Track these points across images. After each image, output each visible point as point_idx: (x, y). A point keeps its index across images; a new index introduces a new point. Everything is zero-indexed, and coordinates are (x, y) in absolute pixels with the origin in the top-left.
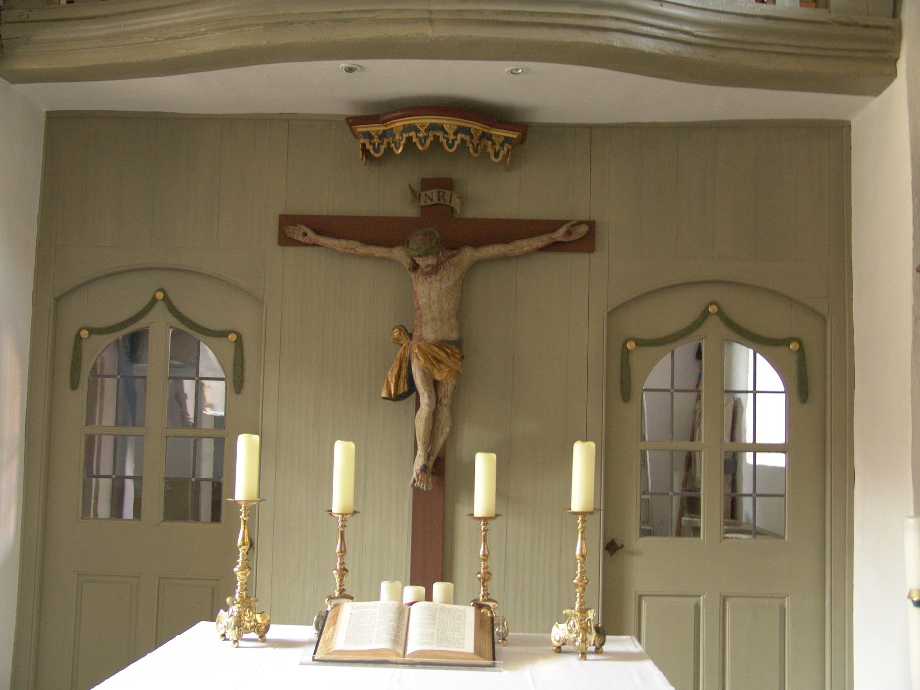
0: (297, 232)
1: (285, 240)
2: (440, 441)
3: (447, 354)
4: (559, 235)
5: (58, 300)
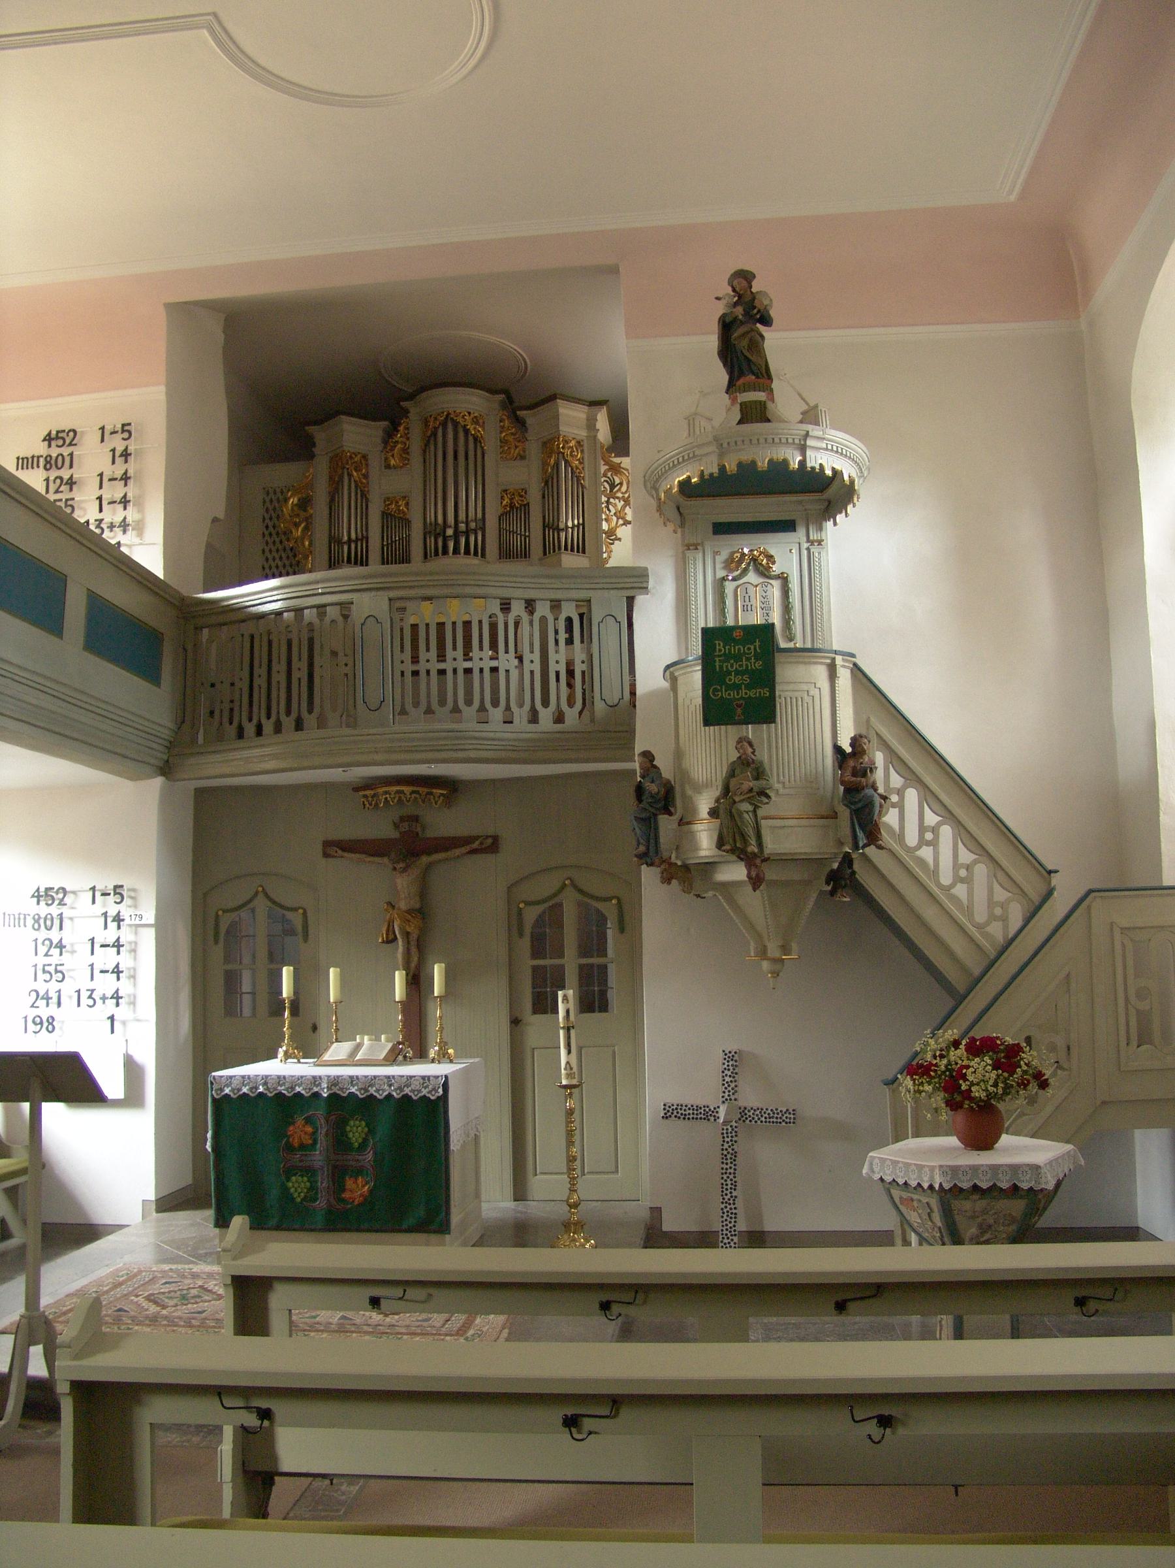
0: (332, 850)
2: (413, 965)
3: (412, 916)
4: (476, 845)
5: (205, 895)
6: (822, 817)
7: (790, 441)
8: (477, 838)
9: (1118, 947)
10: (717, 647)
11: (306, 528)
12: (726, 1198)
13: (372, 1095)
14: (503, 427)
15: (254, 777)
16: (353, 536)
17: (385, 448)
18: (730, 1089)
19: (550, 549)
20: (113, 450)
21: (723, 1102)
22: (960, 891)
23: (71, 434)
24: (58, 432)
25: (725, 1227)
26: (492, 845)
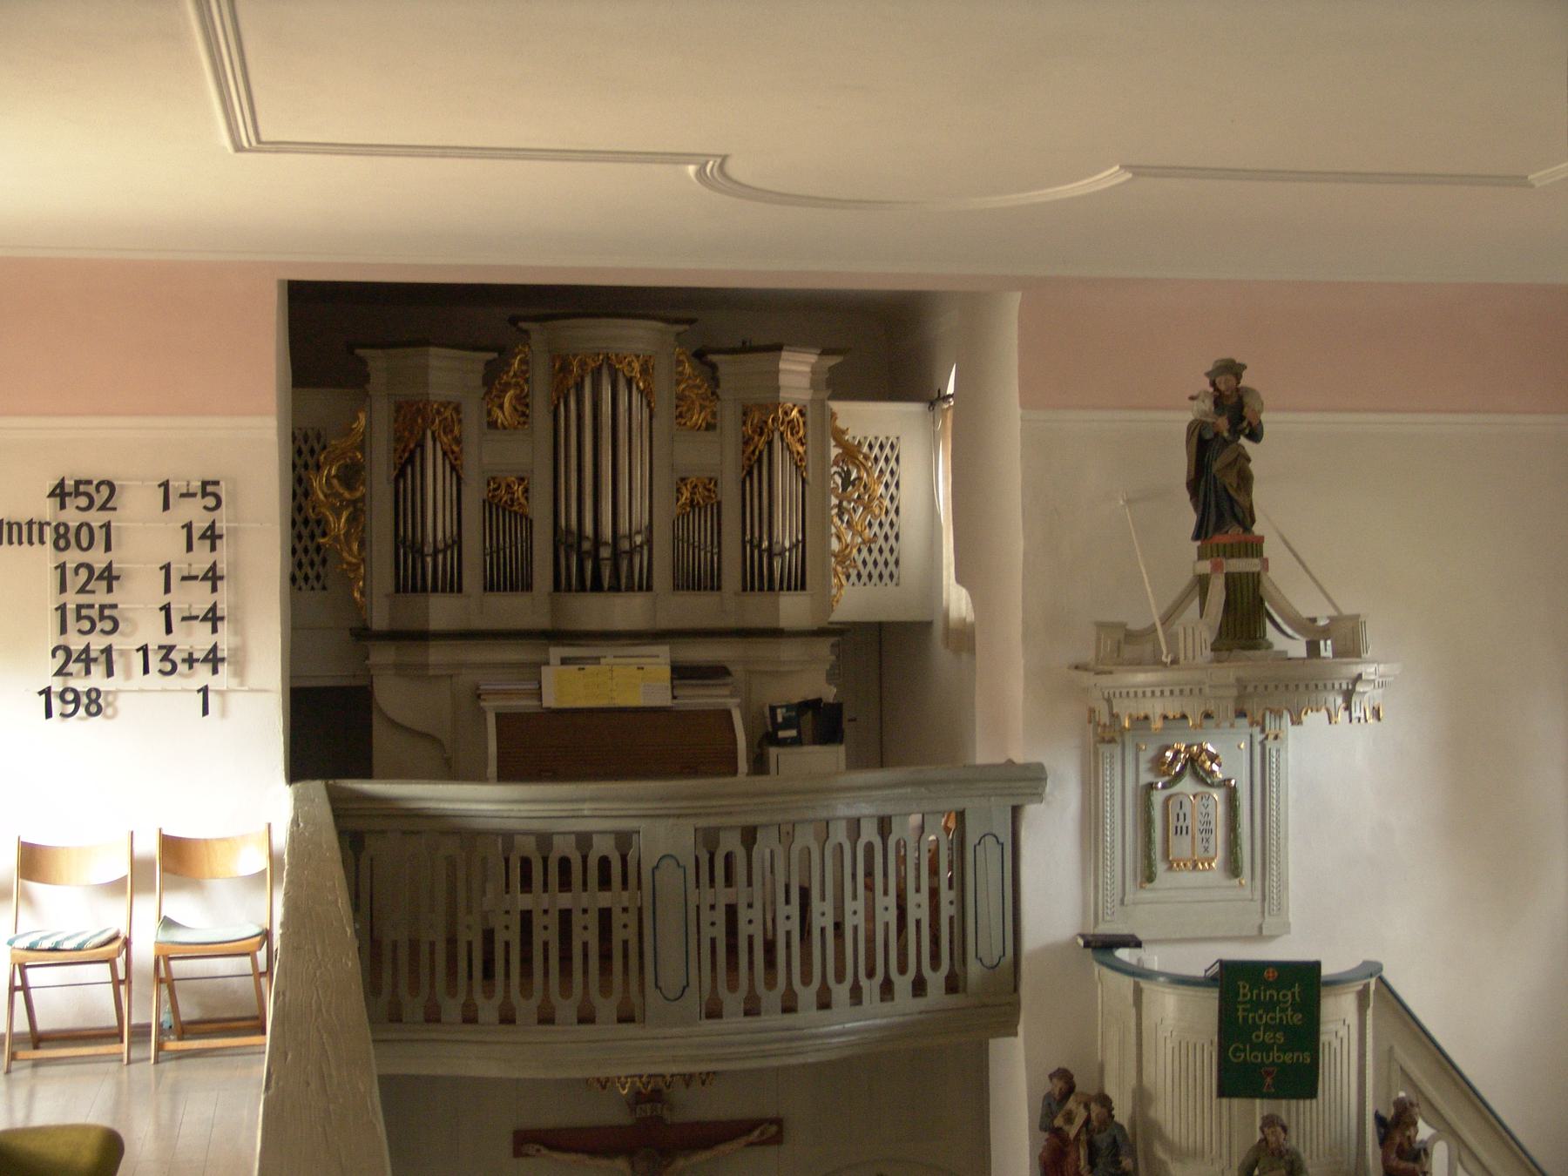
0: (531, 1148)
1: (518, 1153)
10: (1241, 991)
11: (352, 520)
14: (681, 373)
17: (488, 393)
20: (188, 527)
23: (105, 491)
24: (78, 483)
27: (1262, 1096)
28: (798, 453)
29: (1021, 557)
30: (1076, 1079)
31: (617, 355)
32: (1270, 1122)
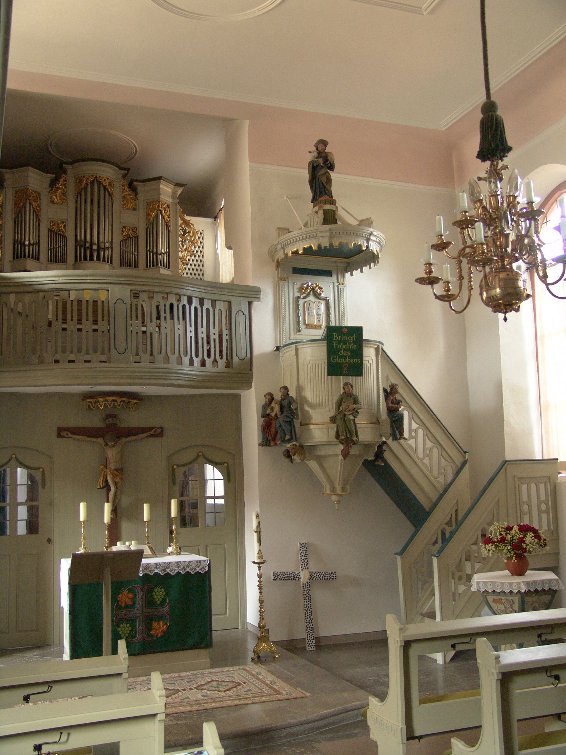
0: (64, 434)
1: (60, 436)
4: (152, 432)
6: (373, 424)
7: (364, 236)
8: (153, 428)
9: (517, 486)
10: (335, 336)
12: (308, 620)
13: (168, 573)
14: (124, 190)
15: (27, 388)
16: (32, 242)
17: (51, 190)
18: (305, 563)
19: (152, 263)
21: (302, 570)
22: (426, 461)
25: (309, 636)
26: (158, 433)
27: (344, 375)
28: (167, 220)
29: (250, 214)
30: (274, 396)
31: (100, 177)
32: (346, 384)
